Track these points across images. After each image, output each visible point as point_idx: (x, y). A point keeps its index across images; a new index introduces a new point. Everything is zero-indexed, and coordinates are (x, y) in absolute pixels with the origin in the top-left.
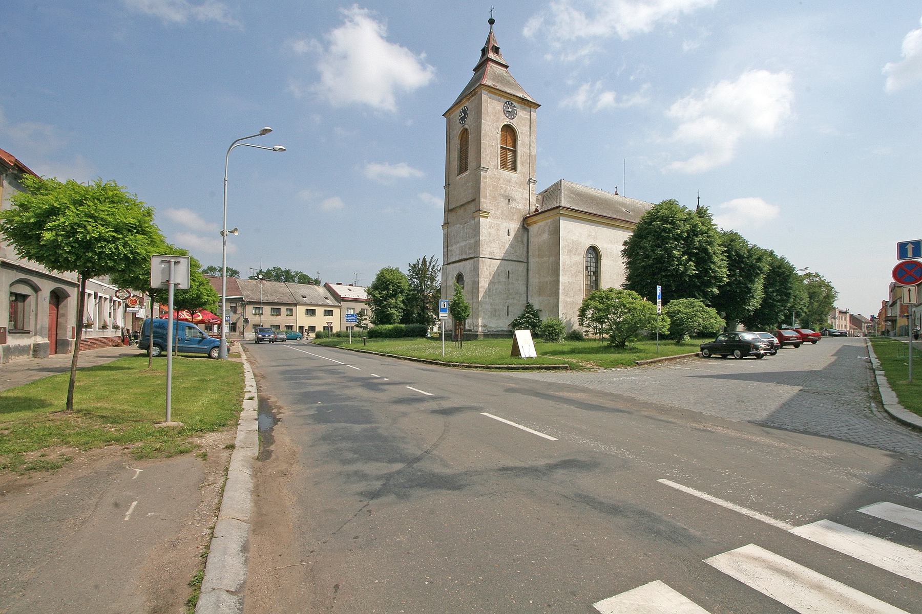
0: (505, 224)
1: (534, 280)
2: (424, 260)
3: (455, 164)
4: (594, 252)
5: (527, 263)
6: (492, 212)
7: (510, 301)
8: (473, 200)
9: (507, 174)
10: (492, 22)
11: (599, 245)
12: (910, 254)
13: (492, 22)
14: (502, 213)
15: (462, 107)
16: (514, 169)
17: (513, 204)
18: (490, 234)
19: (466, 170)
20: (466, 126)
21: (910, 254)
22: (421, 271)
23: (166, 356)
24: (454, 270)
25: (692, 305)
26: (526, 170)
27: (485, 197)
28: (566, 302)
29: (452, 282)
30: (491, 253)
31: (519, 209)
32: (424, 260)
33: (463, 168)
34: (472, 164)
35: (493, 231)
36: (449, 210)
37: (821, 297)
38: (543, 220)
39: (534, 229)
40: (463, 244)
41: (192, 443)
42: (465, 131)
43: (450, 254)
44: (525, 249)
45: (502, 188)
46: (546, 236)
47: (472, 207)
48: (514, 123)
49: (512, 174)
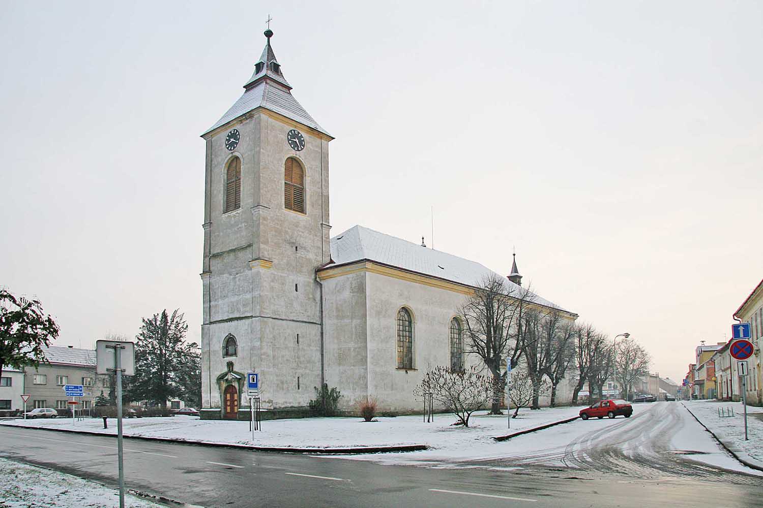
0: (291, 277)
1: (331, 346)
2: (164, 316)
3: (220, 198)
4: (406, 315)
5: (321, 324)
6: (275, 261)
7: (300, 371)
8: (250, 246)
9: (293, 215)
10: (269, 34)
11: (412, 305)
12: (742, 335)
13: (269, 34)
14: (288, 264)
15: (231, 129)
16: (302, 210)
17: (301, 253)
18: (272, 288)
19: (237, 206)
20: (237, 154)
21: (742, 335)
22: (161, 329)
23: (7, 385)
24: (220, 333)
25: (659, 472)
26: (317, 212)
27: (266, 243)
28: (376, 373)
29: (218, 346)
30: (274, 312)
31: (309, 260)
32: (164, 316)
33: (232, 203)
34: (246, 198)
35: (276, 285)
36: (210, 256)
37: (634, 370)
38: (342, 274)
39: (328, 285)
40: (234, 299)
41: (355, 339)
42: (235, 161)
43: (213, 310)
44: (318, 308)
45: (286, 232)
46: (347, 294)
47: (247, 255)
48: (301, 155)
49: (299, 216)
